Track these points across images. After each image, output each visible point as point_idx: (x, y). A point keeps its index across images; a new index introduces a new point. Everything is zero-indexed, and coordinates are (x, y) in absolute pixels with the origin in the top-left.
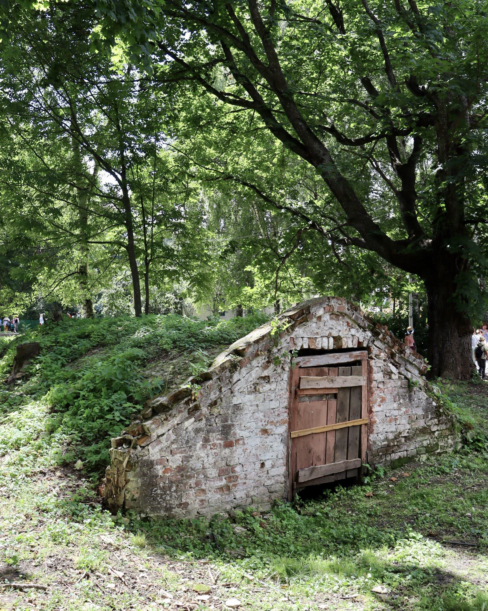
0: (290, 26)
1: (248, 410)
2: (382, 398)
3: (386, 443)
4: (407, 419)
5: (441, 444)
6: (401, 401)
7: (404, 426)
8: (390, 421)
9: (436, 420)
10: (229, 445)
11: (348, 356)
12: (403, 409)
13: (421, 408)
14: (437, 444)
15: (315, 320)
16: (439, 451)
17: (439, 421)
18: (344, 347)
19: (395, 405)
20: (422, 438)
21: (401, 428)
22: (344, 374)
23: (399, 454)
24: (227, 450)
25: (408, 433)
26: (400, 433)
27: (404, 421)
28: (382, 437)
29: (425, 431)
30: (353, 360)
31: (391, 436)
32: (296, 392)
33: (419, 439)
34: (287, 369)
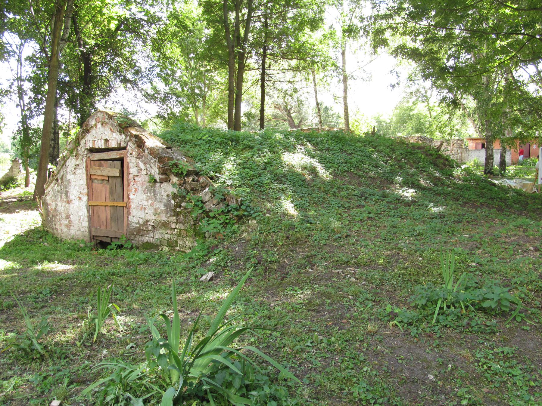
0: (431, 49)
1: (73, 183)
2: (135, 188)
3: (137, 225)
4: (153, 211)
5: (180, 242)
6: (149, 194)
7: (152, 218)
8: (141, 209)
9: (175, 218)
10: (68, 202)
11: (117, 154)
12: (150, 202)
13: (163, 204)
14: (176, 241)
15: (189, 153)
16: (178, 248)
17: (177, 220)
18: (110, 147)
19: (145, 197)
20: (164, 231)
21: (148, 218)
22: (110, 167)
23: (147, 238)
24: (68, 205)
25: (153, 222)
26: (148, 221)
27: (150, 212)
28: (135, 220)
29: (165, 225)
30: (118, 157)
31: (141, 222)
32: (90, 178)
33: (161, 231)
34: (84, 160)
